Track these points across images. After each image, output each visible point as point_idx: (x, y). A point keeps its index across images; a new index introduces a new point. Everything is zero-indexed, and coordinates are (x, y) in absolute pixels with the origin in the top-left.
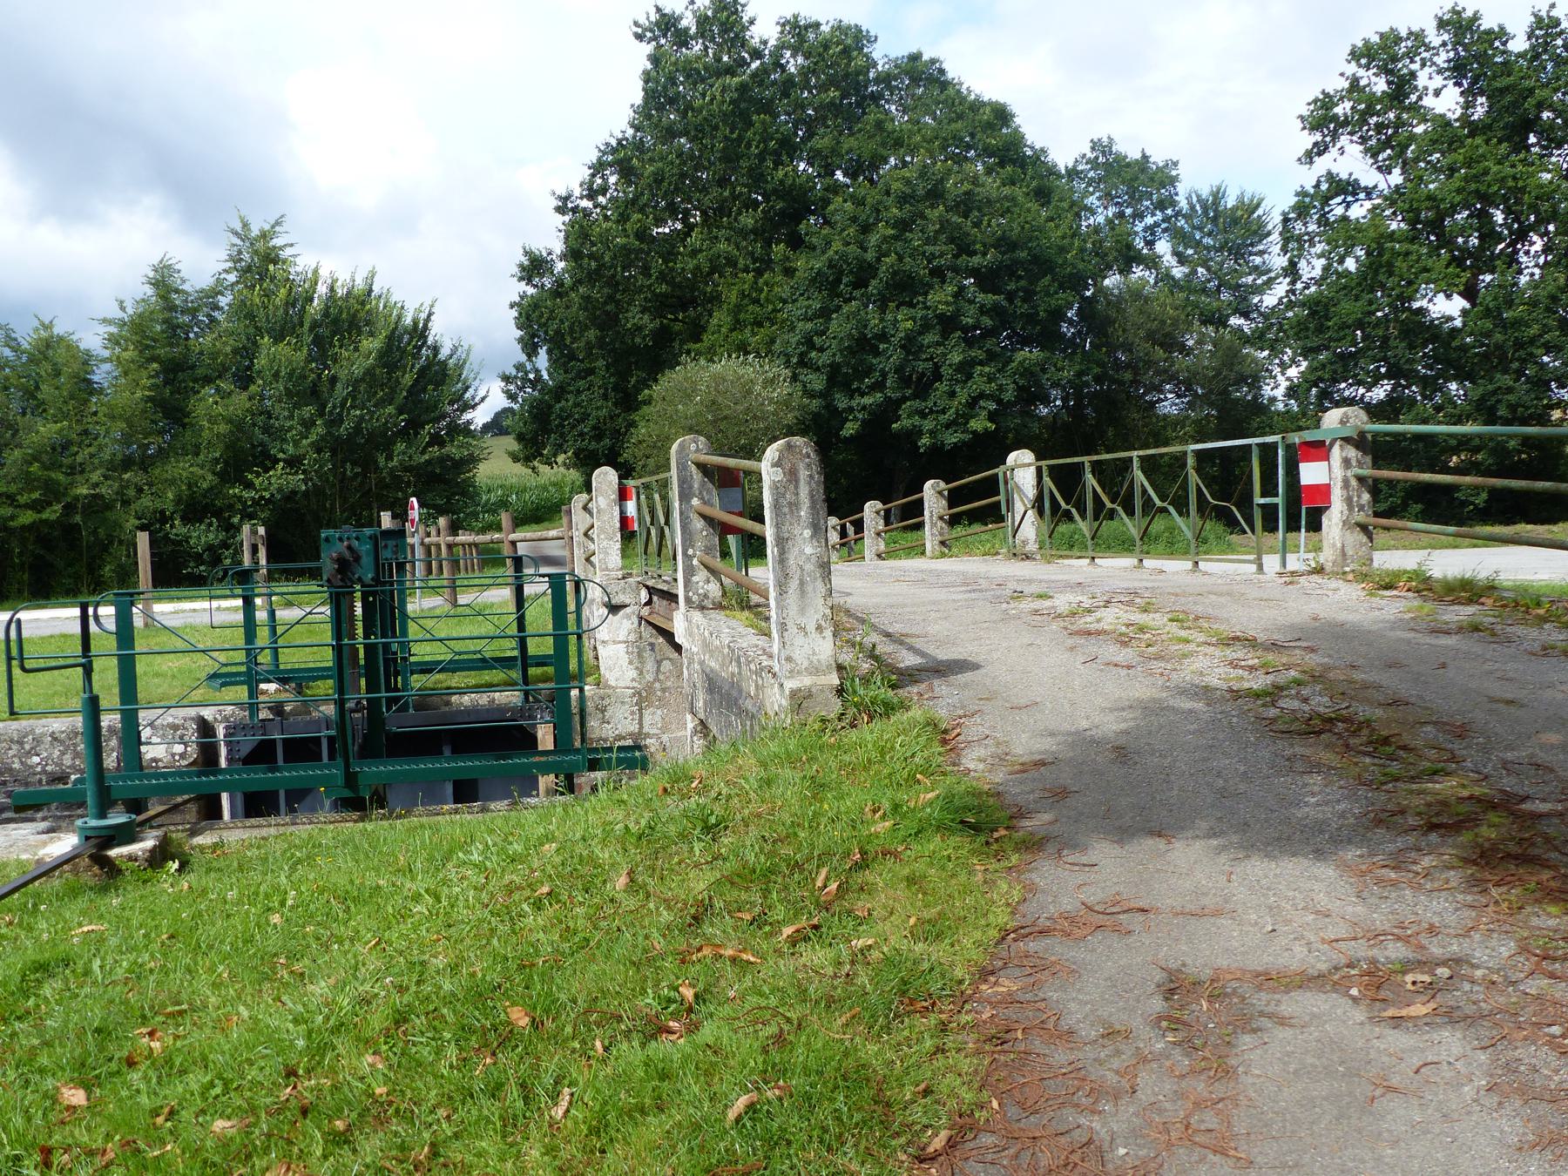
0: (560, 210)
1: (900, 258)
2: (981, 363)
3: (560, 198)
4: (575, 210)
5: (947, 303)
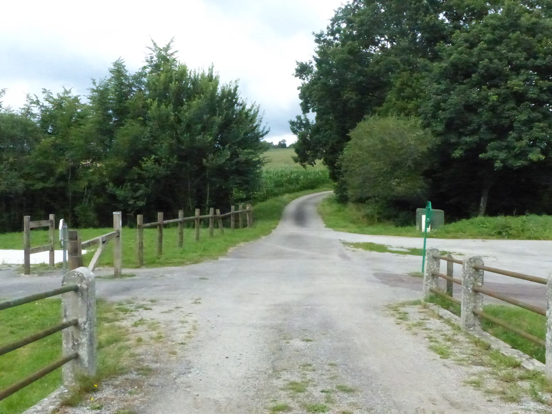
0: (317, 41)
1: (491, 60)
2: (539, 121)
3: (317, 36)
4: (325, 41)
5: (519, 86)
